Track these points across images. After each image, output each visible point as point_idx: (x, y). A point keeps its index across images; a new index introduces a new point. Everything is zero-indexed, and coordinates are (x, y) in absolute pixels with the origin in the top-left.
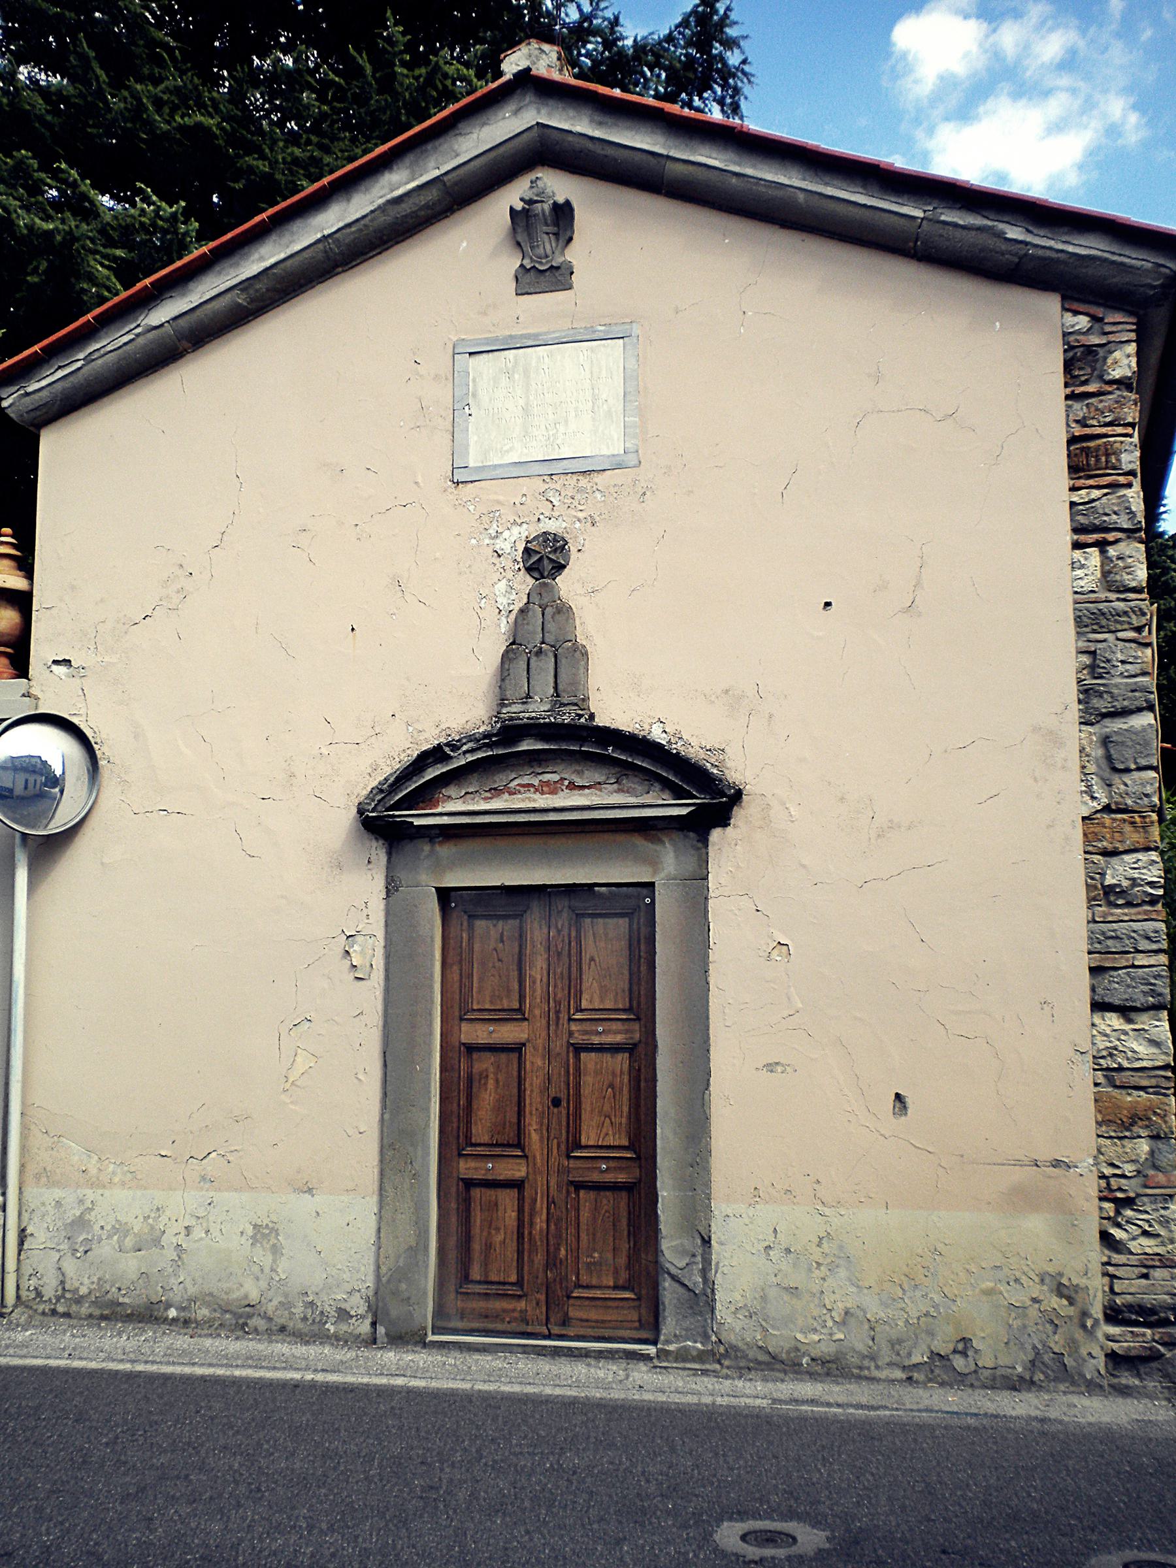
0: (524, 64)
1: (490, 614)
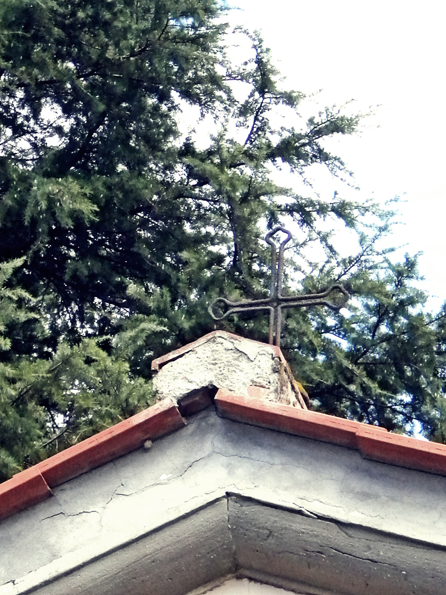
0: (200, 380)
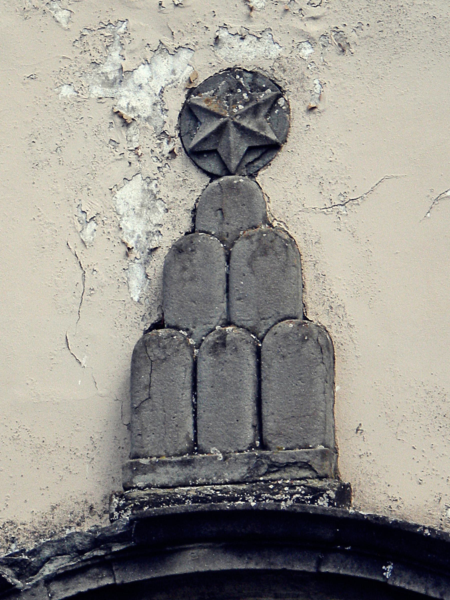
1: (104, 257)
